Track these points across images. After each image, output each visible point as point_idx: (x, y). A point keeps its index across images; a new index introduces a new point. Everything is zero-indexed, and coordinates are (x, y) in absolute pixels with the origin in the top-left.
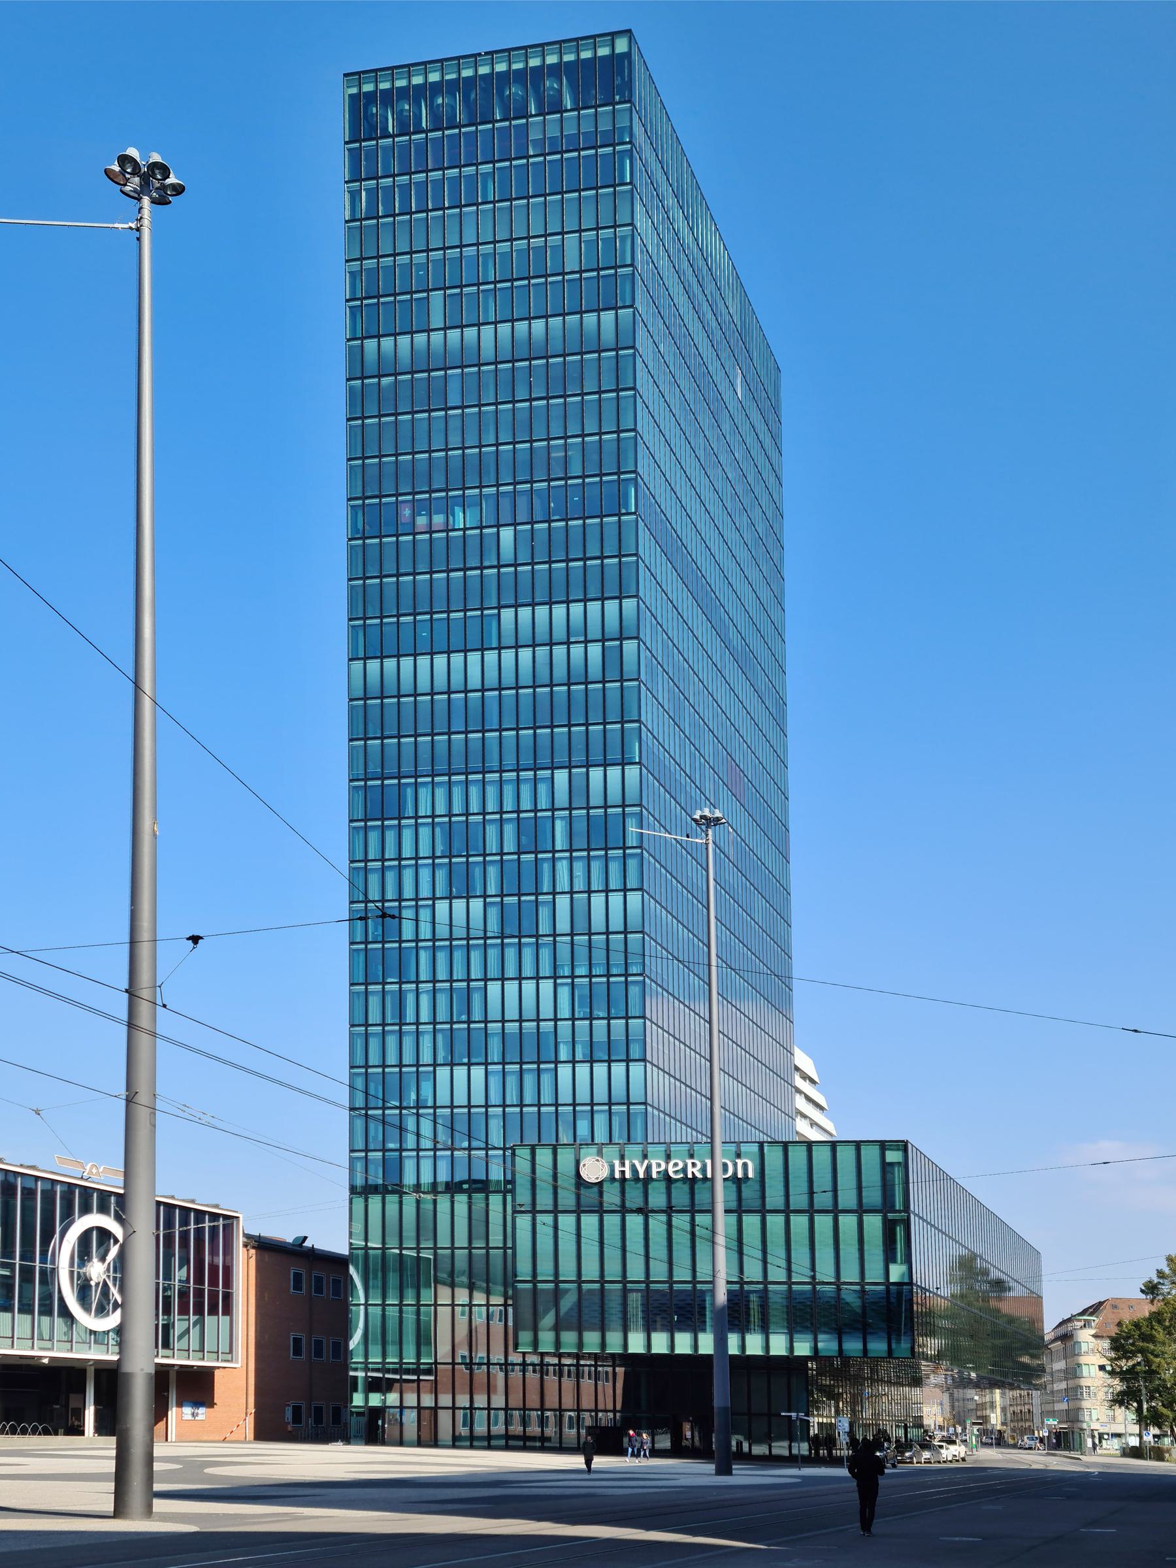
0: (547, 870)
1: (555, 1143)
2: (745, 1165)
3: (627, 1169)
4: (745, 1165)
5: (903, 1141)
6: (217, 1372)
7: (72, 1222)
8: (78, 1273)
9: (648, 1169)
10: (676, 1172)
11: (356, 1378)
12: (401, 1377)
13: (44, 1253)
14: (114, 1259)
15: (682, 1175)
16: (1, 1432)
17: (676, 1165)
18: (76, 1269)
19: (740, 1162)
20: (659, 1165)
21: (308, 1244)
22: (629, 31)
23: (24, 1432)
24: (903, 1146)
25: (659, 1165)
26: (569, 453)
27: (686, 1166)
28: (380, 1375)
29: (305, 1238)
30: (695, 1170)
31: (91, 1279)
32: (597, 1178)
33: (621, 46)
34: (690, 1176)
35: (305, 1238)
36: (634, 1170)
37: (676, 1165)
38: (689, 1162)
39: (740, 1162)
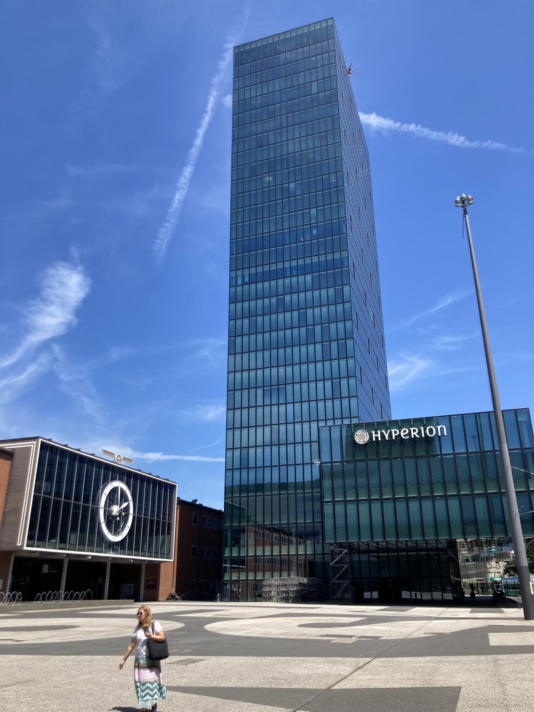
0: (58, 622)
1: (341, 424)
2: (442, 428)
3: (379, 435)
4: (442, 428)
5: (526, 409)
6: (162, 565)
7: (108, 484)
8: (108, 510)
9: (390, 435)
10: (404, 436)
11: (226, 567)
12: (239, 566)
13: (94, 500)
14: (124, 508)
15: (408, 437)
16: (1, 656)
17: (405, 431)
18: (107, 508)
19: (439, 427)
20: (396, 432)
21: (197, 503)
22: (332, 18)
23: (77, 598)
24: (527, 411)
25: (396, 432)
26: (316, 155)
27: (410, 431)
28: (241, 566)
29: (196, 500)
30: (415, 433)
31: (113, 512)
32: (364, 442)
33: (330, 23)
34: (413, 437)
35: (196, 500)
36: (383, 436)
37: (405, 431)
38: (412, 429)
39: (439, 427)
